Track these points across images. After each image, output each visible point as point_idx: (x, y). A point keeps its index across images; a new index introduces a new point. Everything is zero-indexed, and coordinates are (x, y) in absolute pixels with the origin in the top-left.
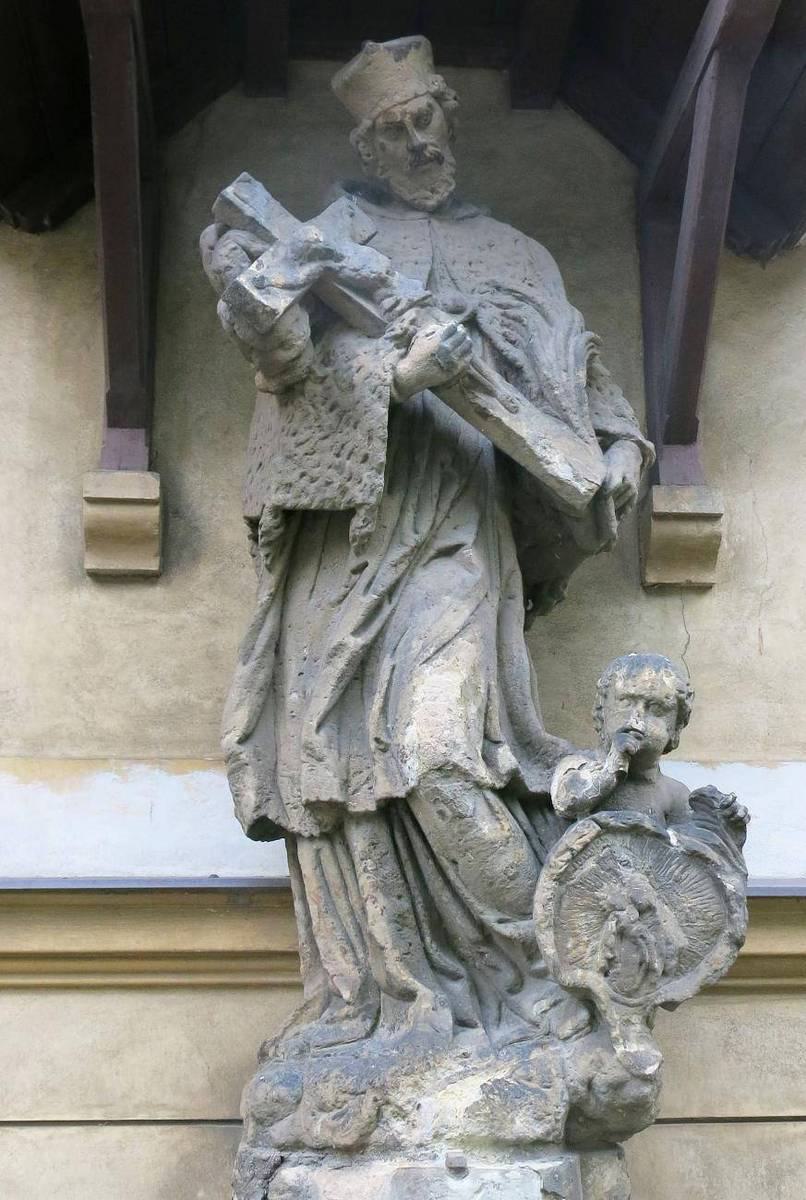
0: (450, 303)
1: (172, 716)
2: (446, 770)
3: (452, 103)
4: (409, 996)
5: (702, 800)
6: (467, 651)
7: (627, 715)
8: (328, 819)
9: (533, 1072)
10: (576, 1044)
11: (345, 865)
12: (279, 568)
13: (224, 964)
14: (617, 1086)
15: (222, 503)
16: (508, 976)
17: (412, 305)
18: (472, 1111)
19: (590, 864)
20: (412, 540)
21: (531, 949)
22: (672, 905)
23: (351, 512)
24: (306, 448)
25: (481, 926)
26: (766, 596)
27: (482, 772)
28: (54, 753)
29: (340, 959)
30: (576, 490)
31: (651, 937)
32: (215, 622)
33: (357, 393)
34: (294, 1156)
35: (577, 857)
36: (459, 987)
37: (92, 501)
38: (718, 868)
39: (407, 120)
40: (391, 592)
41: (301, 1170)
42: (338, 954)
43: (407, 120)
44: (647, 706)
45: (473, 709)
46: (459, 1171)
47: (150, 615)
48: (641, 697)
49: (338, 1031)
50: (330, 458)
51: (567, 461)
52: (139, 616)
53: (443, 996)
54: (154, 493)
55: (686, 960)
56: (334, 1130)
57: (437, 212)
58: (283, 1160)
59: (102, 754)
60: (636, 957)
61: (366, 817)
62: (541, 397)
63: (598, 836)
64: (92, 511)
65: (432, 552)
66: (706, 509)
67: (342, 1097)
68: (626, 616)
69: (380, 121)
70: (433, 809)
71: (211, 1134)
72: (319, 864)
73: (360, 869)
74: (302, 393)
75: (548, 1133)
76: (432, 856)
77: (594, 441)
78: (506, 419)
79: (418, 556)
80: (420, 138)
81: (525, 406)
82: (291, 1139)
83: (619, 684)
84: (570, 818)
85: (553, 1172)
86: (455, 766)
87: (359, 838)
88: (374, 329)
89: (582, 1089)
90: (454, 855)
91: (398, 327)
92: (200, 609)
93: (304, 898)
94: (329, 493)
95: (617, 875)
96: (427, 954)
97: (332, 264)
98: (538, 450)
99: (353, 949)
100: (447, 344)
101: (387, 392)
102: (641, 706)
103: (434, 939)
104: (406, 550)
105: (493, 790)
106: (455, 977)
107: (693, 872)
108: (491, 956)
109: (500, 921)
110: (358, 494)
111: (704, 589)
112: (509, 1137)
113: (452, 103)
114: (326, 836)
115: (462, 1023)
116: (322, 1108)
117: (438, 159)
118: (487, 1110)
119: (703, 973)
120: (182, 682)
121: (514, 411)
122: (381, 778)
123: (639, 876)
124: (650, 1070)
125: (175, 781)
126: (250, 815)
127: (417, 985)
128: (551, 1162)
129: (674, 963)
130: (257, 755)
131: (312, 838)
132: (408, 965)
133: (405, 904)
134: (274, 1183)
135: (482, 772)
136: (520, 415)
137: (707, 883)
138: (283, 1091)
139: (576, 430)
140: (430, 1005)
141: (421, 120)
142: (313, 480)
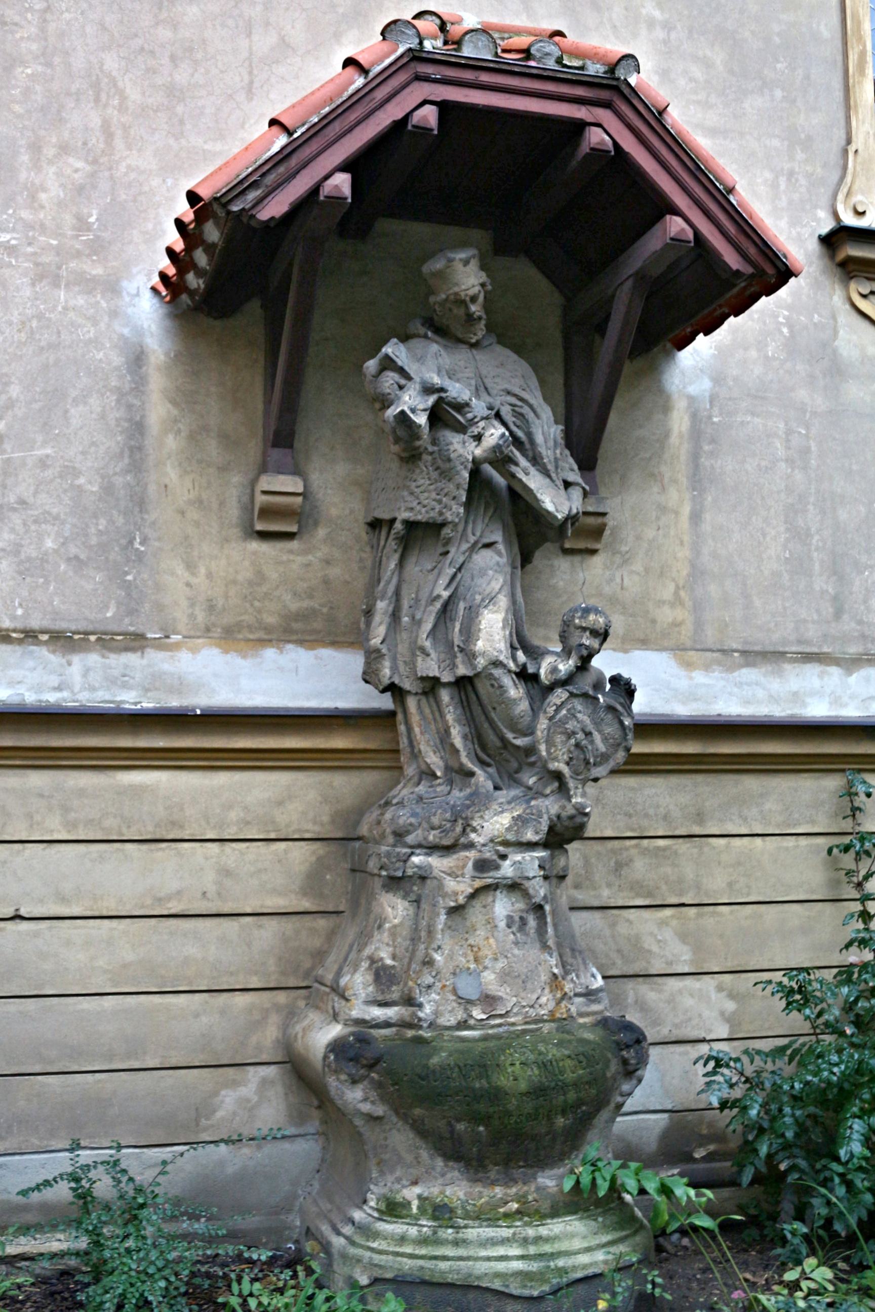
1: (303, 616)
2: (497, 664)
3: (489, 288)
4: (472, 774)
5: (616, 680)
6: (503, 601)
7: (582, 637)
8: (428, 685)
10: (551, 798)
13: (319, 756)
14: (571, 818)
16: (515, 765)
17: (483, 419)
19: (564, 712)
20: (472, 539)
21: (530, 750)
22: (600, 732)
23: (443, 525)
24: (422, 488)
25: (503, 739)
26: (627, 556)
27: (512, 665)
28: (240, 636)
30: (556, 517)
31: (590, 747)
33: (452, 464)
34: (418, 851)
35: (559, 708)
36: (490, 770)
38: (621, 714)
39: (468, 299)
42: (431, 754)
45: (507, 633)
47: (292, 557)
49: (435, 791)
50: (434, 495)
51: (552, 501)
55: (604, 758)
58: (412, 853)
59: (266, 637)
60: (582, 756)
62: (536, 460)
69: (452, 297)
70: (488, 683)
71: (333, 847)
76: (481, 704)
77: (562, 487)
78: (524, 479)
79: (473, 548)
81: (533, 470)
83: (577, 621)
84: (551, 688)
85: (542, 857)
86: (501, 662)
87: (445, 696)
88: (461, 429)
90: (496, 705)
91: (475, 431)
92: (319, 554)
94: (432, 514)
97: (444, 395)
98: (539, 495)
100: (501, 442)
101: (470, 466)
102: (588, 633)
106: (489, 765)
107: (610, 716)
108: (506, 754)
110: (449, 516)
111: (593, 552)
113: (489, 288)
114: (425, 693)
115: (497, 788)
116: (433, 828)
117: (480, 318)
119: (611, 764)
120: (311, 597)
121: (527, 474)
123: (586, 718)
124: (588, 810)
125: (311, 653)
127: (476, 769)
128: (541, 854)
131: (416, 694)
132: (470, 759)
134: (409, 864)
135: (512, 665)
137: (616, 721)
138: (413, 820)
139: (553, 481)
140: (482, 778)
141: (474, 299)
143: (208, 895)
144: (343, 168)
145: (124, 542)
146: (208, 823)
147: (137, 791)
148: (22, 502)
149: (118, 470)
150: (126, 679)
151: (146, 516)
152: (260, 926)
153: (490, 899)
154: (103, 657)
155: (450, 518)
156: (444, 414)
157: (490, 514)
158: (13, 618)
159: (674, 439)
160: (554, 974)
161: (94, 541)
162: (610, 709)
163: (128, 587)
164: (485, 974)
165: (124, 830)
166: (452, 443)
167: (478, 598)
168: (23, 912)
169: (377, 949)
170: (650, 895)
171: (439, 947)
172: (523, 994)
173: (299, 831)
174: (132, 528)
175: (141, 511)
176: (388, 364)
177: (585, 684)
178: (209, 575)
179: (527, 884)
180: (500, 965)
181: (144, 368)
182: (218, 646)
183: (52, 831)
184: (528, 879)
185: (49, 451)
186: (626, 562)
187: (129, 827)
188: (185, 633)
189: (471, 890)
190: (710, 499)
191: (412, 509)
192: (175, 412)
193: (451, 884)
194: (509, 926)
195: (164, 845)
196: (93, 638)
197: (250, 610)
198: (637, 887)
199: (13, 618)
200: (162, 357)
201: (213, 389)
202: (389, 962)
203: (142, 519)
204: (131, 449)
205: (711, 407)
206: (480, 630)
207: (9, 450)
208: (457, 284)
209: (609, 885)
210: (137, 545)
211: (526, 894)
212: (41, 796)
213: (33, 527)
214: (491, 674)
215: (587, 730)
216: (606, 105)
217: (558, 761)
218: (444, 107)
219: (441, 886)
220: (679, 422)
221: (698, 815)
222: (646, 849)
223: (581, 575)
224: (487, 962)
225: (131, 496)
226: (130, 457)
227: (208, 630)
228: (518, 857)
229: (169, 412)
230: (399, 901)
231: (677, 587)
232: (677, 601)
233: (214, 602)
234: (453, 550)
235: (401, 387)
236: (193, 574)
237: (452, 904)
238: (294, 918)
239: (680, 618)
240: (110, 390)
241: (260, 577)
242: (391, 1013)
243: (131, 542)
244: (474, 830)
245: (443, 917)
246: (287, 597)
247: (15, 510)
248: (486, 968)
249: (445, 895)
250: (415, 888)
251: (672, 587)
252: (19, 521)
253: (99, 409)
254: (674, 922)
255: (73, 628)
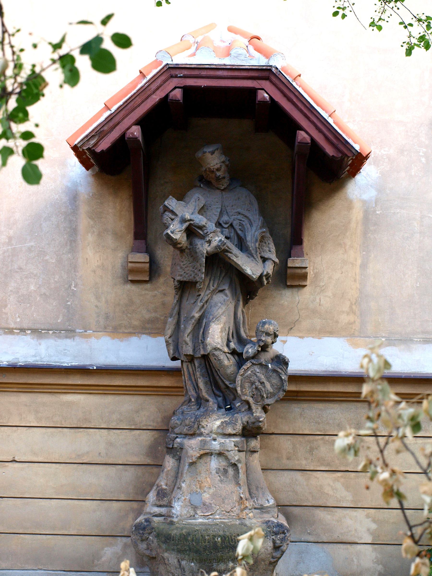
0: (225, 221)
1: (152, 321)
2: (216, 349)
3: (227, 163)
4: (207, 401)
9: (234, 419)
11: (193, 367)
12: (179, 293)
14: (254, 423)
15: (166, 259)
18: (218, 427)
19: (249, 372)
20: (212, 288)
22: (269, 382)
23: (197, 282)
24: (185, 266)
25: (226, 385)
26: (323, 288)
29: (192, 391)
30: (253, 277)
31: (263, 389)
32: (164, 294)
34: (179, 436)
35: (246, 371)
36: (220, 399)
37: (130, 262)
38: (280, 373)
40: (206, 302)
41: (181, 439)
42: (192, 390)
43: (215, 170)
44: (266, 334)
46: (215, 440)
47: (147, 292)
48: (264, 332)
50: (191, 269)
52: (143, 292)
53: (216, 401)
54: (148, 260)
55: (272, 395)
56: (188, 430)
57: (223, 190)
58: (177, 437)
61: (199, 358)
63: (251, 365)
64: (130, 265)
65: (217, 291)
66: (304, 266)
67: (191, 423)
68: (281, 294)
72: (188, 368)
73: (197, 370)
74: (185, 252)
75: (237, 433)
77: (260, 261)
80: (218, 174)
82: (179, 432)
86: (218, 348)
87: (197, 363)
88: (203, 237)
89: (245, 423)
92: (160, 290)
93: (184, 376)
95: (255, 374)
96: (213, 390)
97: (192, 222)
98: (243, 267)
99: (195, 389)
102: (264, 335)
103: (215, 387)
104: (210, 291)
105: (228, 353)
106: (220, 397)
109: (230, 384)
111: (305, 286)
112: (227, 433)
113: (227, 163)
117: (224, 178)
118: (222, 427)
119: (276, 398)
120: (156, 312)
121: (237, 257)
122: (202, 350)
124: (261, 420)
126: (172, 356)
129: (269, 395)
130: (173, 341)
133: (208, 379)
134: (175, 441)
135: (226, 350)
136: (239, 258)
137: (278, 377)
139: (255, 259)
141: (218, 170)
142: (187, 274)
143: (101, 454)
144: (137, 123)
145: (66, 286)
146: (102, 420)
147: (70, 404)
148: (20, 268)
149: (64, 252)
150: (66, 351)
151: (77, 274)
152: (126, 470)
153: (209, 459)
154: (56, 341)
155: (198, 280)
156: (192, 231)
157: (223, 275)
158: (15, 323)
159: (353, 225)
160: (241, 497)
161: (53, 286)
162: (274, 371)
163: (68, 308)
164: (204, 494)
165: (63, 422)
166: (197, 245)
167: (211, 317)
168: (16, 459)
169: (160, 481)
170: (328, 465)
171: (184, 481)
172: (222, 505)
173: (146, 425)
174: (71, 279)
175: (75, 272)
176: (166, 209)
177: (264, 358)
178: (107, 302)
179: (226, 453)
180: (211, 491)
181: (77, 202)
182: (109, 336)
183: (30, 422)
184: (228, 451)
185: (32, 244)
186: (322, 291)
187: (65, 421)
188: (95, 330)
189: (199, 455)
190: (372, 256)
191: (181, 275)
192: (92, 223)
193: (191, 452)
194: (217, 473)
195: (82, 430)
196: (51, 332)
197: (126, 319)
198: (321, 460)
199: (15, 323)
200: (86, 196)
201: (110, 211)
202: (164, 487)
203: (75, 275)
204: (71, 241)
205: (376, 206)
206: (209, 333)
207: (14, 244)
208: (209, 164)
209: (306, 459)
210: (73, 288)
211: (227, 458)
212: (26, 405)
213: (25, 280)
214: (214, 354)
215: (262, 381)
216: (266, 78)
217: (247, 396)
218: (186, 90)
219: (187, 452)
220: (357, 214)
221: (358, 424)
222: (327, 441)
223: (297, 298)
224: (205, 489)
225: (70, 264)
226: (70, 245)
227: (105, 328)
228: (223, 441)
229: (89, 223)
230: (171, 459)
231: (351, 304)
232: (351, 311)
233: (109, 315)
234: (202, 294)
235: (172, 220)
236: (99, 301)
237: (191, 461)
238: (143, 467)
239: (352, 320)
240: (61, 214)
241: (131, 302)
242: (163, 510)
243: (70, 286)
244: (203, 427)
245: (187, 467)
246: (144, 312)
247: (17, 272)
248: (205, 492)
249: (188, 457)
250: (178, 453)
251: (348, 303)
252: (18, 277)
253: (56, 223)
254: (342, 480)
255: (43, 327)
